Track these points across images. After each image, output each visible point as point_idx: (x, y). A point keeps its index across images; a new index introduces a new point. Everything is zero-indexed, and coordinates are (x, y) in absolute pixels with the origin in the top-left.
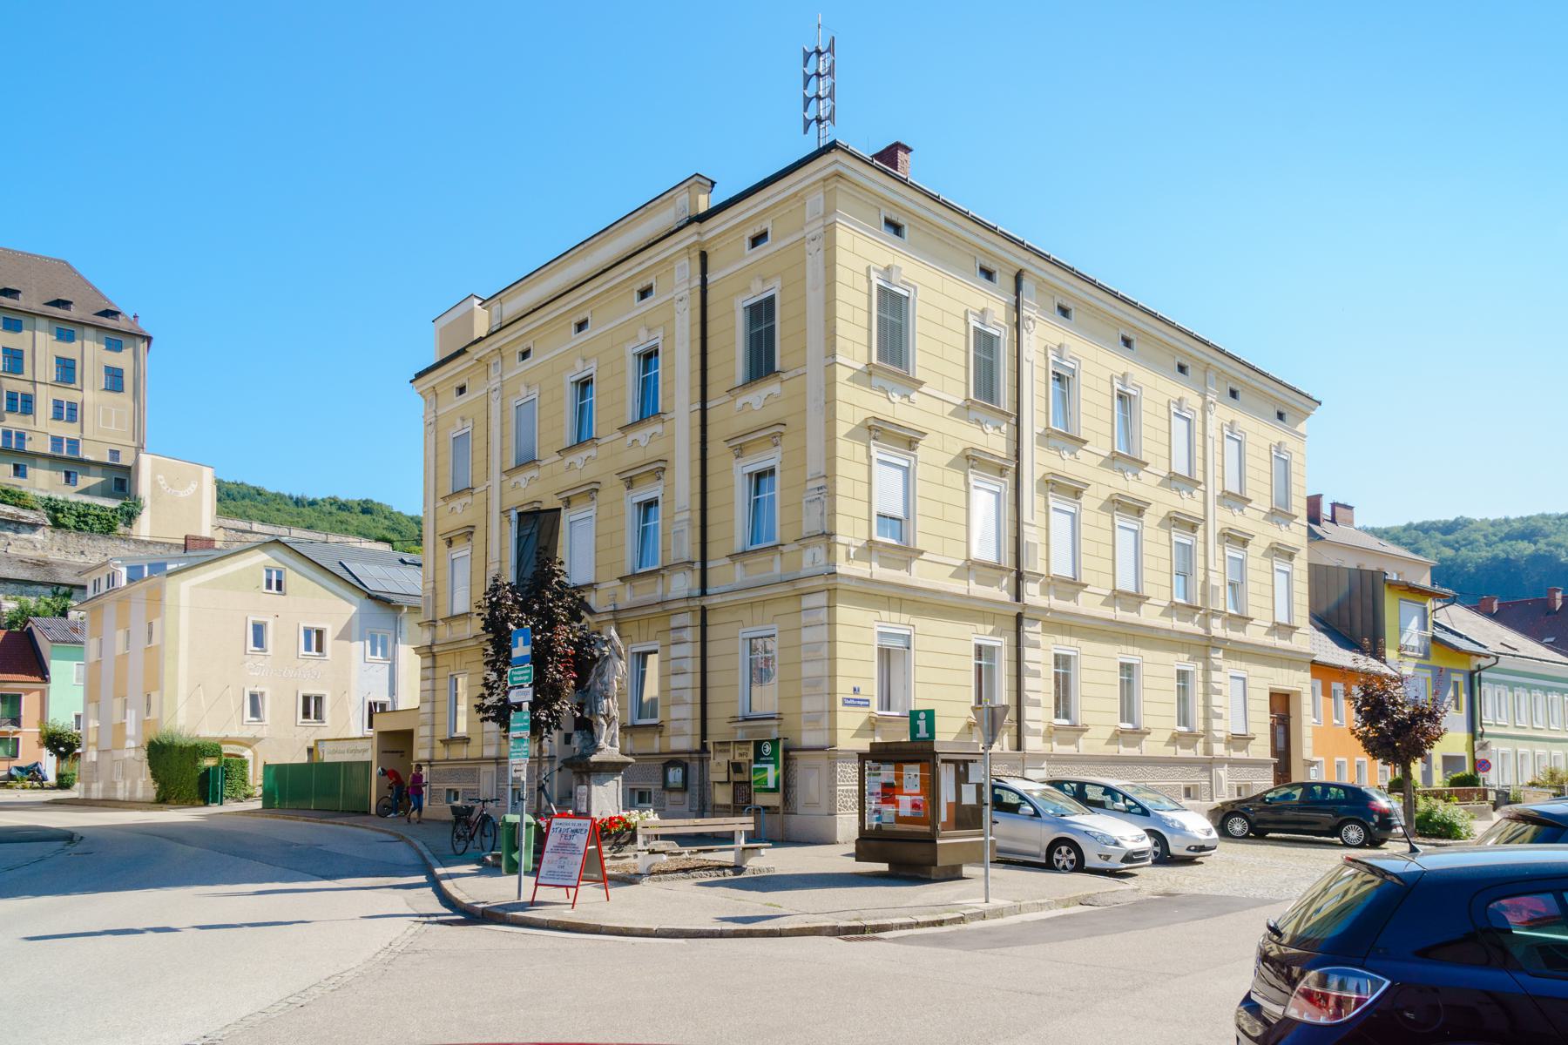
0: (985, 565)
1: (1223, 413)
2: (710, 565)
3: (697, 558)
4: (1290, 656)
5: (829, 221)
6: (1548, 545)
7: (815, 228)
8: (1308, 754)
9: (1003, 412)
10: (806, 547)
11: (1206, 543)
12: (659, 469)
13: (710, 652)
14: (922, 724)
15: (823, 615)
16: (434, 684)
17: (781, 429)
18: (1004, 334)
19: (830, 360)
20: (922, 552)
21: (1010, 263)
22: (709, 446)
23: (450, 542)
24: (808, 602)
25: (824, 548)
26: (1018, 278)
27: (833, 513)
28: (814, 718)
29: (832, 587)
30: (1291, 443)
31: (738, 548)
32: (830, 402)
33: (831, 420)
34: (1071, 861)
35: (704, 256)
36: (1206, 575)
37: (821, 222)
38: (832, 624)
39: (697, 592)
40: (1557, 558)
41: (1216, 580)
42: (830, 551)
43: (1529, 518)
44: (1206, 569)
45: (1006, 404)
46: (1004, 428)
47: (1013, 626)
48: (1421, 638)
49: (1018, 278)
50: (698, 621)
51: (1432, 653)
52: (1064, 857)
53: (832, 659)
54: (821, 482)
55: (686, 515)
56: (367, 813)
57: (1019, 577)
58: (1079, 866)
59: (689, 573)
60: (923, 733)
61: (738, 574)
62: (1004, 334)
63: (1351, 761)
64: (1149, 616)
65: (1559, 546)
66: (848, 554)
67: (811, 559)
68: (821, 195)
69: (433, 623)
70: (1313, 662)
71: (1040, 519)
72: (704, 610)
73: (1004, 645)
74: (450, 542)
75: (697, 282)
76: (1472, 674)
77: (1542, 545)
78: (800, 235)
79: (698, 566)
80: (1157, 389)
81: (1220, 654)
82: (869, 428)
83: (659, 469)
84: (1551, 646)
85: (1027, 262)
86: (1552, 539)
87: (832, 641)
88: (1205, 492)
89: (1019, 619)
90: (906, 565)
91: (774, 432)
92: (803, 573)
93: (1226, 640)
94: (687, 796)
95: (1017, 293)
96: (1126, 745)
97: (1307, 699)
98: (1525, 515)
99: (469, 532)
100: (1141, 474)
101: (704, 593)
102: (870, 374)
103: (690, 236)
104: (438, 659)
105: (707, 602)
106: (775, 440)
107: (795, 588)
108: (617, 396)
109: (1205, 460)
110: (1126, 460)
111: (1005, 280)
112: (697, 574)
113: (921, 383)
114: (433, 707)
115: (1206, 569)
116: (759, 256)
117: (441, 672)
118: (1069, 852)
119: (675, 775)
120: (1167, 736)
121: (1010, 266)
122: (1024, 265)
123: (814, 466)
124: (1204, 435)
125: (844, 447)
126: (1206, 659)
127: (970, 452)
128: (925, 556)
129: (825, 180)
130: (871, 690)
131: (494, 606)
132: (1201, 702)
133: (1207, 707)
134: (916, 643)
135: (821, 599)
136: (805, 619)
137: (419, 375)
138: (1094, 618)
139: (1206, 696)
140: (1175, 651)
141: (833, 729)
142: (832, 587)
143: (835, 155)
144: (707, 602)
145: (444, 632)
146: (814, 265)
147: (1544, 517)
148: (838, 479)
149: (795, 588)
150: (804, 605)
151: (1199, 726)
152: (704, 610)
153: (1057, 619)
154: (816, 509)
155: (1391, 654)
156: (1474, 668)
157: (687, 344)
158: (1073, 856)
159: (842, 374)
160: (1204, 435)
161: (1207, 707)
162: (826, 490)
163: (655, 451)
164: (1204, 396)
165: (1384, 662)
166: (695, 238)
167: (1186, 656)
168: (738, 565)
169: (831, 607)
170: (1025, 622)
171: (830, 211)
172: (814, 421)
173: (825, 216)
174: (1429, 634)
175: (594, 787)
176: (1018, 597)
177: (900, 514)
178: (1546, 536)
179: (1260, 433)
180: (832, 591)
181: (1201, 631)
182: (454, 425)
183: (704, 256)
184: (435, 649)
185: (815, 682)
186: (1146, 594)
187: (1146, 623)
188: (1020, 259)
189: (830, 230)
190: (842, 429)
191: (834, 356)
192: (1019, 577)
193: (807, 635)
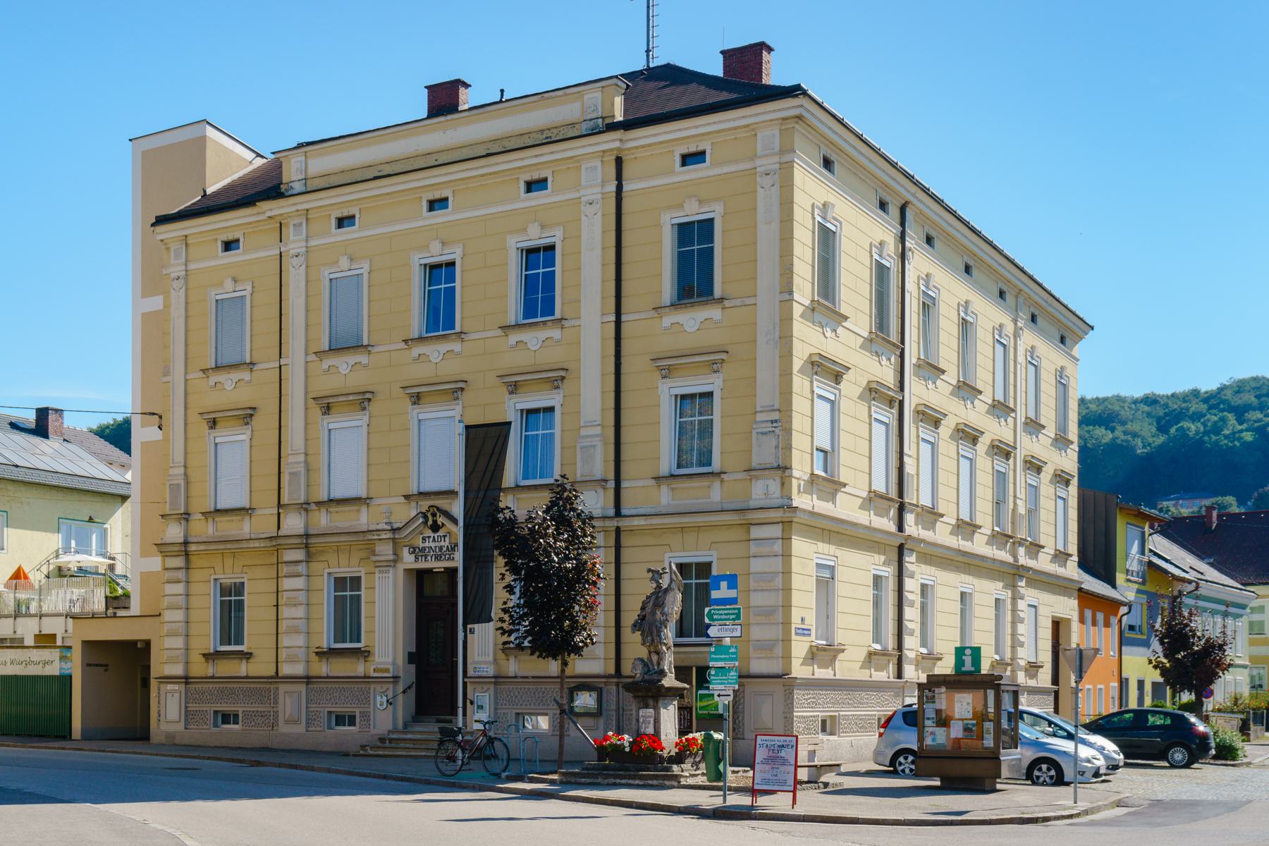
0: (882, 497)
1: (1029, 338)
2: (624, 484)
3: (611, 476)
4: (1066, 584)
5: (786, 158)
6: (1125, 433)
7: (770, 163)
8: (477, 658)
9: (889, 342)
10: (757, 478)
11: (1015, 471)
12: (557, 378)
13: (624, 574)
14: (968, 660)
15: (778, 547)
16: (187, 588)
17: (723, 356)
18: (891, 263)
19: (786, 297)
20: (845, 485)
21: (898, 194)
22: (623, 360)
23: (213, 424)
24: (756, 532)
25: (778, 480)
26: (903, 210)
27: (789, 447)
28: (766, 647)
29: (788, 519)
30: (1070, 371)
31: (664, 469)
32: (785, 339)
33: (787, 355)
34: (1051, 777)
35: (619, 162)
36: (1015, 504)
37: (776, 159)
38: (787, 555)
39: (612, 512)
40: (1133, 449)
41: (1022, 510)
42: (785, 484)
43: (1105, 399)
44: (1015, 496)
45: (894, 337)
46: (893, 359)
47: (895, 557)
48: (1140, 562)
49: (903, 210)
50: (612, 542)
51: (1148, 578)
52: (1044, 772)
53: (787, 590)
54: (775, 416)
55: (598, 430)
56: (62, 733)
57: (901, 509)
58: (1059, 781)
59: (601, 491)
60: (968, 667)
61: (665, 497)
62: (891, 263)
63: (1095, 687)
64: (979, 545)
65: (1135, 435)
66: (799, 486)
67: (762, 490)
68: (777, 132)
69: (186, 516)
70: (1080, 590)
71: (914, 446)
72: (618, 531)
73: (889, 572)
74: (213, 424)
75: (612, 187)
76: (1175, 598)
77: (1118, 433)
78: (748, 165)
79: (612, 484)
80: (990, 315)
81: (1022, 583)
82: (812, 363)
83: (557, 378)
84: (1211, 565)
85: (914, 195)
86: (1129, 426)
87: (787, 573)
88: (1015, 419)
89: (901, 548)
90: (832, 497)
91: (714, 359)
92: (752, 504)
93: (1029, 569)
94: (601, 721)
95: (903, 224)
96: (823, 666)
97: (1075, 625)
98: (1101, 396)
99: (247, 416)
100: (976, 402)
101: (618, 513)
102: (813, 310)
103: (611, 141)
104: (193, 559)
105: (623, 523)
106: (714, 367)
107: (744, 517)
108: (490, 290)
109: (1015, 386)
110: (967, 390)
111: (894, 211)
112: (611, 493)
113: (846, 318)
114: (187, 616)
115: (1015, 496)
116: (687, 177)
117: (196, 575)
118: (1049, 769)
119: (585, 700)
120: (862, 655)
121: (906, 204)
122: (910, 198)
123: (766, 395)
124: (1015, 361)
125: (800, 383)
126: (1014, 587)
127: (874, 385)
128: (847, 489)
129: (784, 119)
130: (811, 622)
131: (573, 540)
132: (1009, 631)
133: (1014, 635)
134: (841, 574)
135: (776, 531)
136: (754, 549)
137: (162, 220)
138: (949, 548)
139: (1014, 623)
140: (993, 579)
141: (787, 657)
142: (788, 519)
143: (801, 100)
144: (623, 523)
145: (203, 529)
146: (766, 198)
147: (1119, 399)
148: (794, 414)
149: (744, 517)
150: (753, 536)
151: (1008, 655)
152: (618, 531)
153: (930, 550)
154: (770, 442)
155: (1120, 578)
156: (1176, 593)
157: (598, 251)
158: (1053, 773)
159: (797, 310)
160: (1015, 361)
161: (1014, 635)
162: (780, 424)
163: (553, 357)
164: (1015, 321)
165: (1114, 586)
166: (617, 144)
167: (1001, 584)
168: (664, 488)
169: (786, 539)
170: (906, 552)
171: (787, 149)
172: (766, 354)
173: (782, 152)
174: (1146, 559)
175: (663, 711)
176: (901, 528)
177: (827, 447)
178: (1123, 423)
179: (1051, 357)
180: (787, 525)
181: (1011, 560)
182: (221, 284)
183: (619, 162)
184: (193, 548)
185: (769, 612)
186: (978, 523)
187: (939, 542)
188: (907, 192)
189: (786, 171)
190: (797, 364)
191: (791, 292)
192: (901, 509)
193: (756, 565)
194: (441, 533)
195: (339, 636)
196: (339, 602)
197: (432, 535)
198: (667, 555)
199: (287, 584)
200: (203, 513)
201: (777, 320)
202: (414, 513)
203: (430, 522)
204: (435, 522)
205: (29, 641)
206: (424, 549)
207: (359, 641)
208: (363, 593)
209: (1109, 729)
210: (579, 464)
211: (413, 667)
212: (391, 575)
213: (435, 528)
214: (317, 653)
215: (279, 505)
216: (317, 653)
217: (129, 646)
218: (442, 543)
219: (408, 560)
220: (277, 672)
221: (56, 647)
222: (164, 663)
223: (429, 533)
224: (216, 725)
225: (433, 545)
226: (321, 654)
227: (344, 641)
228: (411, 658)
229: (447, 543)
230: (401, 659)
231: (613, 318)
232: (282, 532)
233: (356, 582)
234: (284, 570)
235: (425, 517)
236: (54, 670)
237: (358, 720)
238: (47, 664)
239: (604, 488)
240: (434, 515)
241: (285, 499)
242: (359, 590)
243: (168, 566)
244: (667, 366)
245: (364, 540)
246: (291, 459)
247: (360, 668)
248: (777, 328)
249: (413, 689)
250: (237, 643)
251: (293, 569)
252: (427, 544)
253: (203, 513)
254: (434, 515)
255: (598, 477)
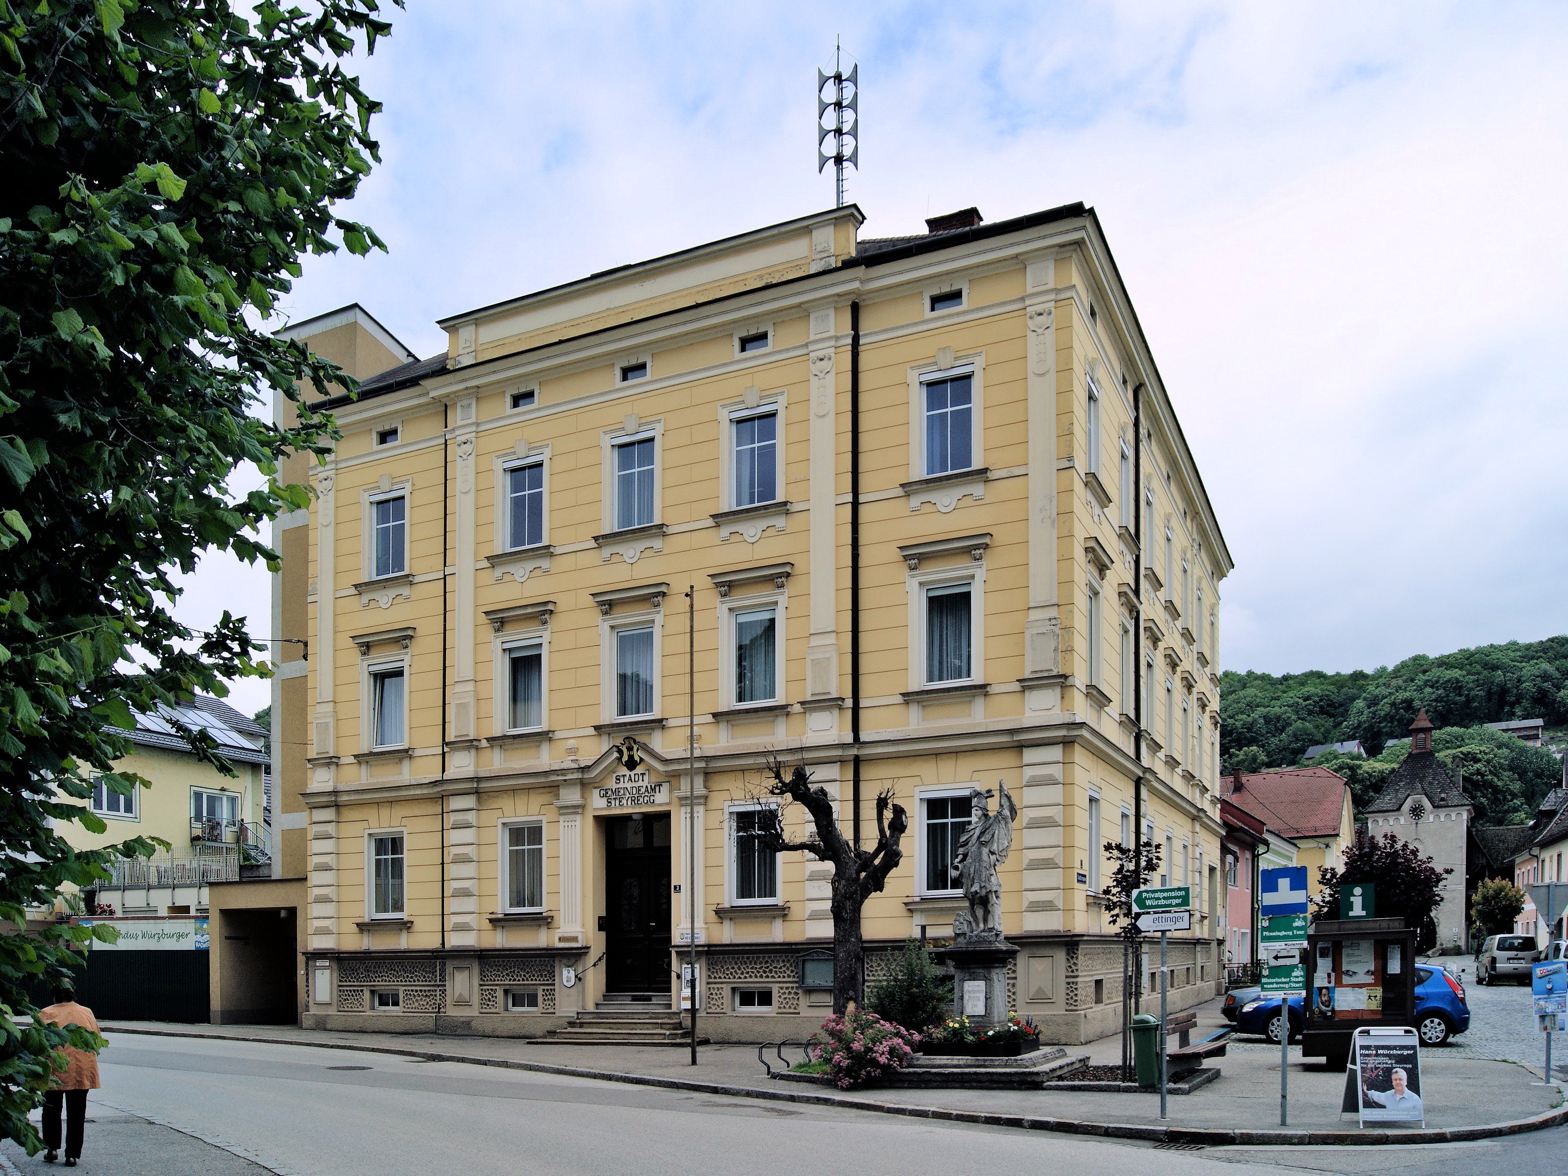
3: (848, 693)
91: (975, 547)
166: (856, 285)
194: (639, 770)
195: (518, 899)
196: (516, 858)
197: (628, 773)
198: (918, 789)
199: (454, 836)
200: (355, 756)
201: (1054, 493)
202: (605, 748)
203: (625, 758)
204: (631, 757)
205: (163, 912)
206: (617, 790)
207: (773, 894)
208: (544, 846)
209: (885, 949)
210: (809, 681)
211: (603, 934)
212: (578, 823)
213: (632, 764)
214: (491, 920)
215: (445, 743)
216: (491, 920)
217: (271, 914)
218: (640, 783)
219: (598, 804)
220: (706, 1042)
221: (190, 918)
222: (315, 934)
223: (624, 770)
224: (373, 1008)
225: (629, 785)
226: (495, 922)
227: (386, 911)
228: (603, 924)
229: (646, 783)
230: (592, 924)
231: (850, 498)
232: (448, 775)
233: (535, 833)
234: (451, 819)
235: (620, 752)
236: (187, 944)
237: (540, 999)
238: (183, 937)
239: (840, 708)
240: (630, 749)
241: (450, 737)
242: (541, 843)
243: (315, 819)
244: (916, 556)
245: (548, 784)
246: (459, 688)
247: (542, 939)
248: (1054, 503)
249: (604, 961)
250: (532, 905)
251: (460, 817)
252: (621, 785)
253: (355, 756)
254: (630, 749)
255: (834, 695)
